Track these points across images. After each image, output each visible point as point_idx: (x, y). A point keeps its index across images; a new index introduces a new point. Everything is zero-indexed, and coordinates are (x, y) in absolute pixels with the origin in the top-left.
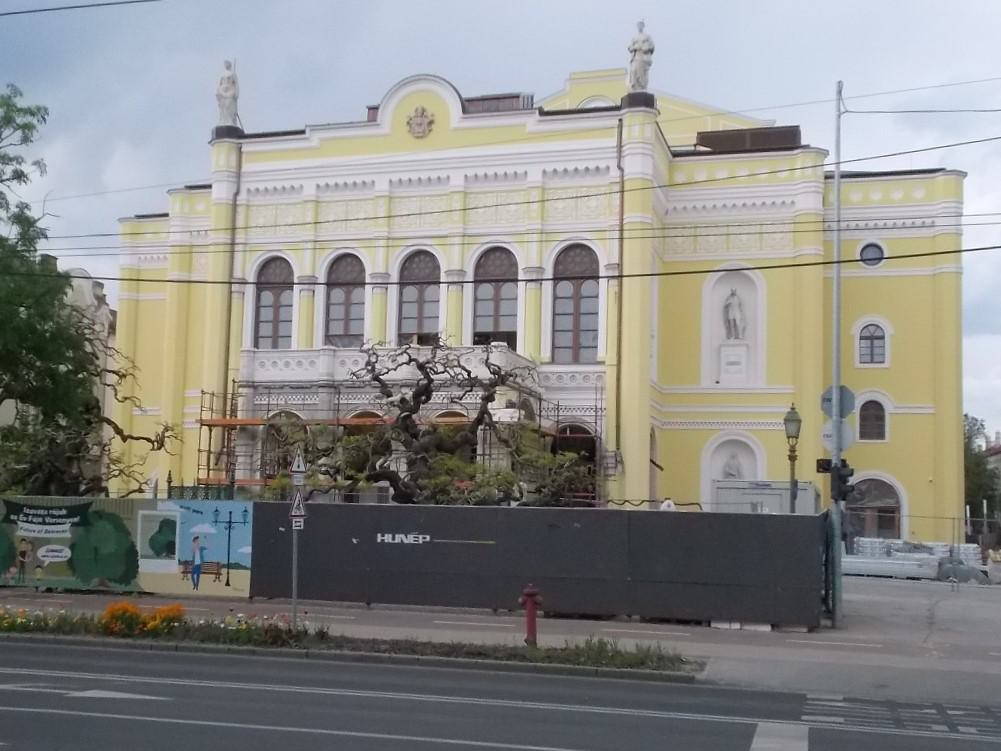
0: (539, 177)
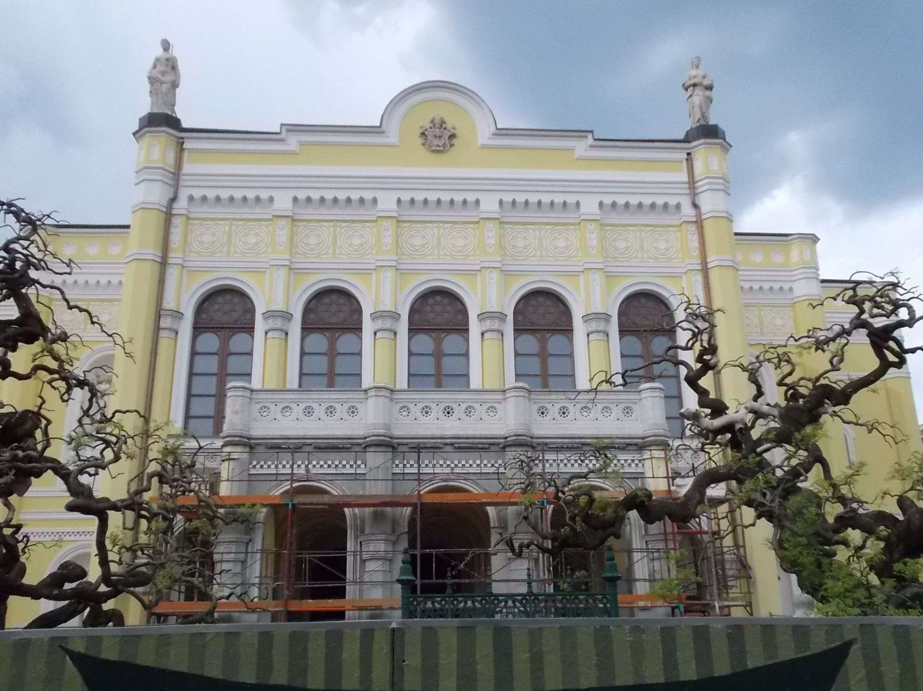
0: (289, 205)
